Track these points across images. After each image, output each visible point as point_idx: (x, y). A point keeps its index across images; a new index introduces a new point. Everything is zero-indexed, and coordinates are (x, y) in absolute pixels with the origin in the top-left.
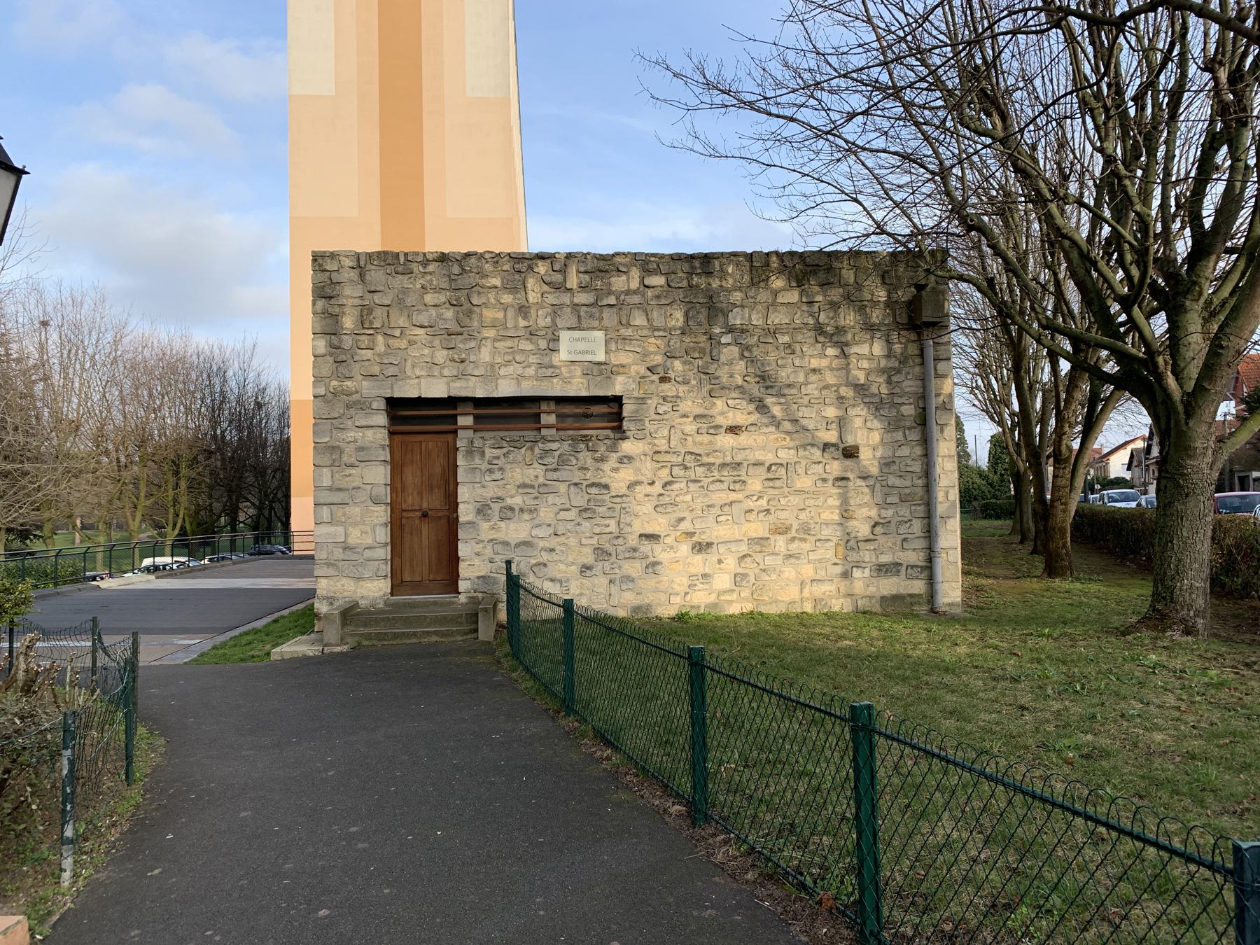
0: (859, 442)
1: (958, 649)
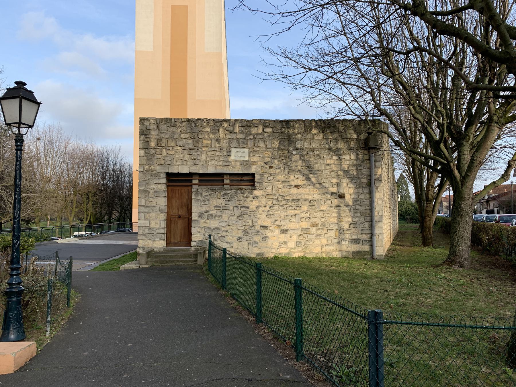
0: (345, 192)
1: (374, 271)
